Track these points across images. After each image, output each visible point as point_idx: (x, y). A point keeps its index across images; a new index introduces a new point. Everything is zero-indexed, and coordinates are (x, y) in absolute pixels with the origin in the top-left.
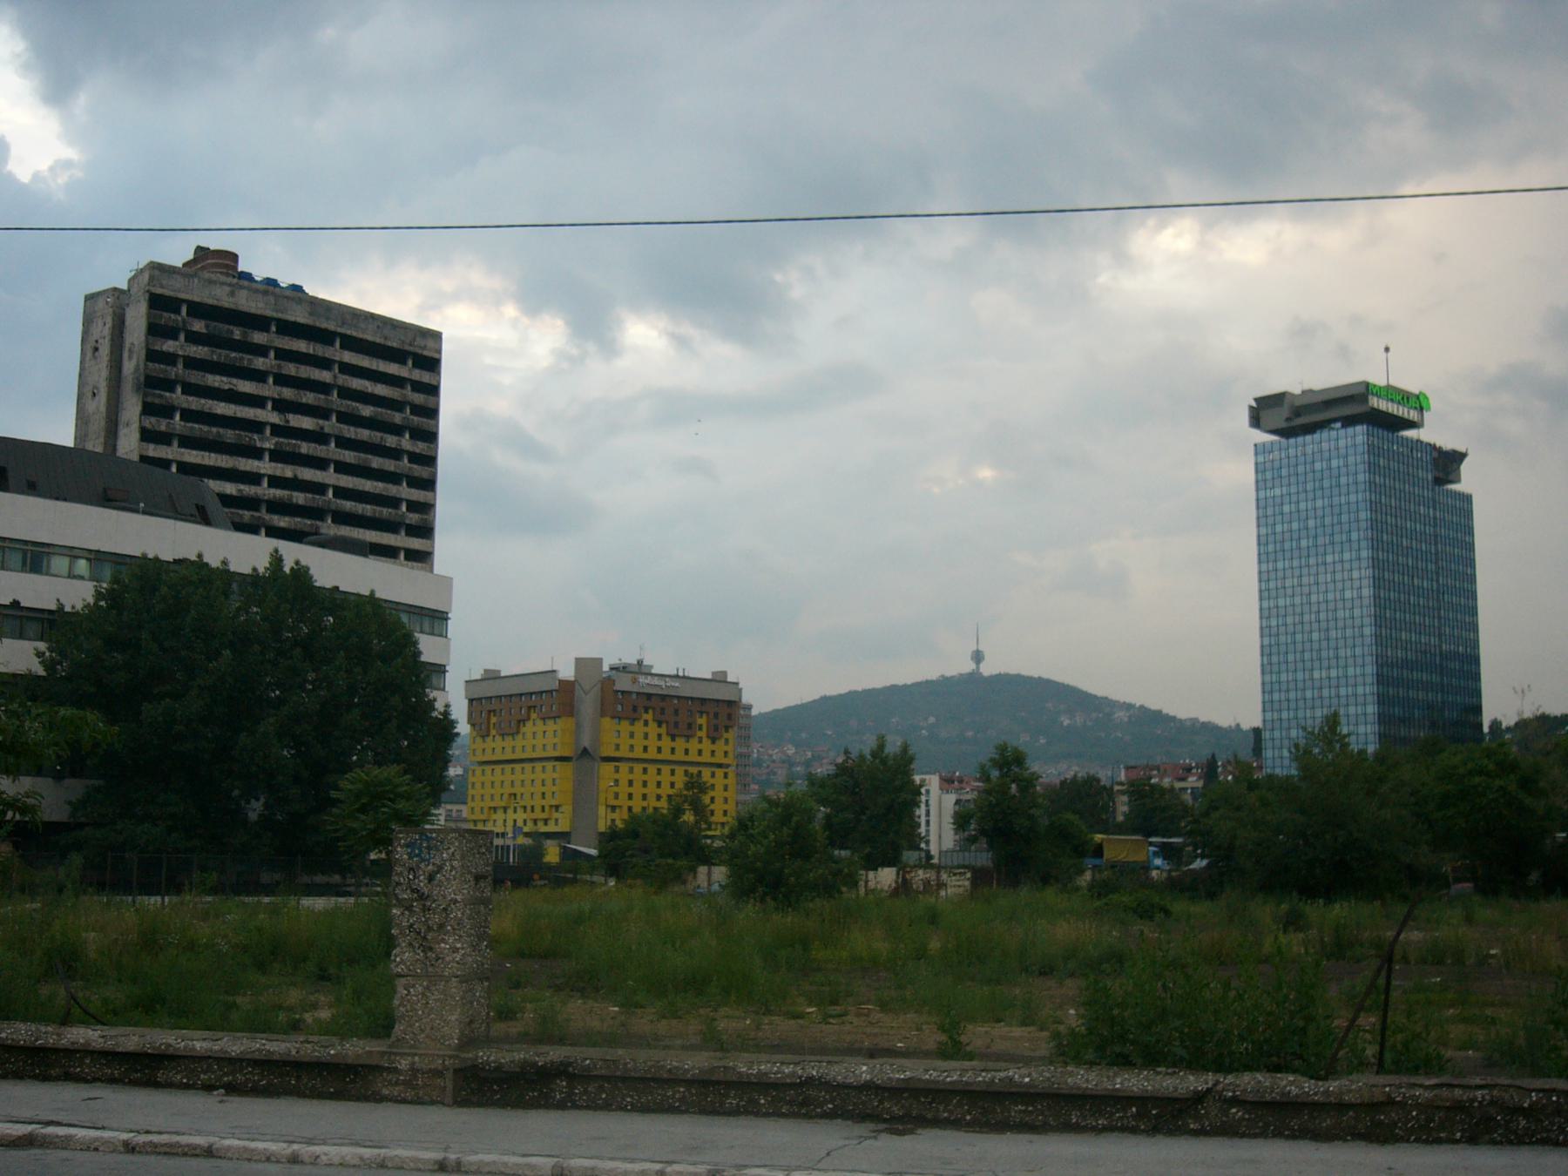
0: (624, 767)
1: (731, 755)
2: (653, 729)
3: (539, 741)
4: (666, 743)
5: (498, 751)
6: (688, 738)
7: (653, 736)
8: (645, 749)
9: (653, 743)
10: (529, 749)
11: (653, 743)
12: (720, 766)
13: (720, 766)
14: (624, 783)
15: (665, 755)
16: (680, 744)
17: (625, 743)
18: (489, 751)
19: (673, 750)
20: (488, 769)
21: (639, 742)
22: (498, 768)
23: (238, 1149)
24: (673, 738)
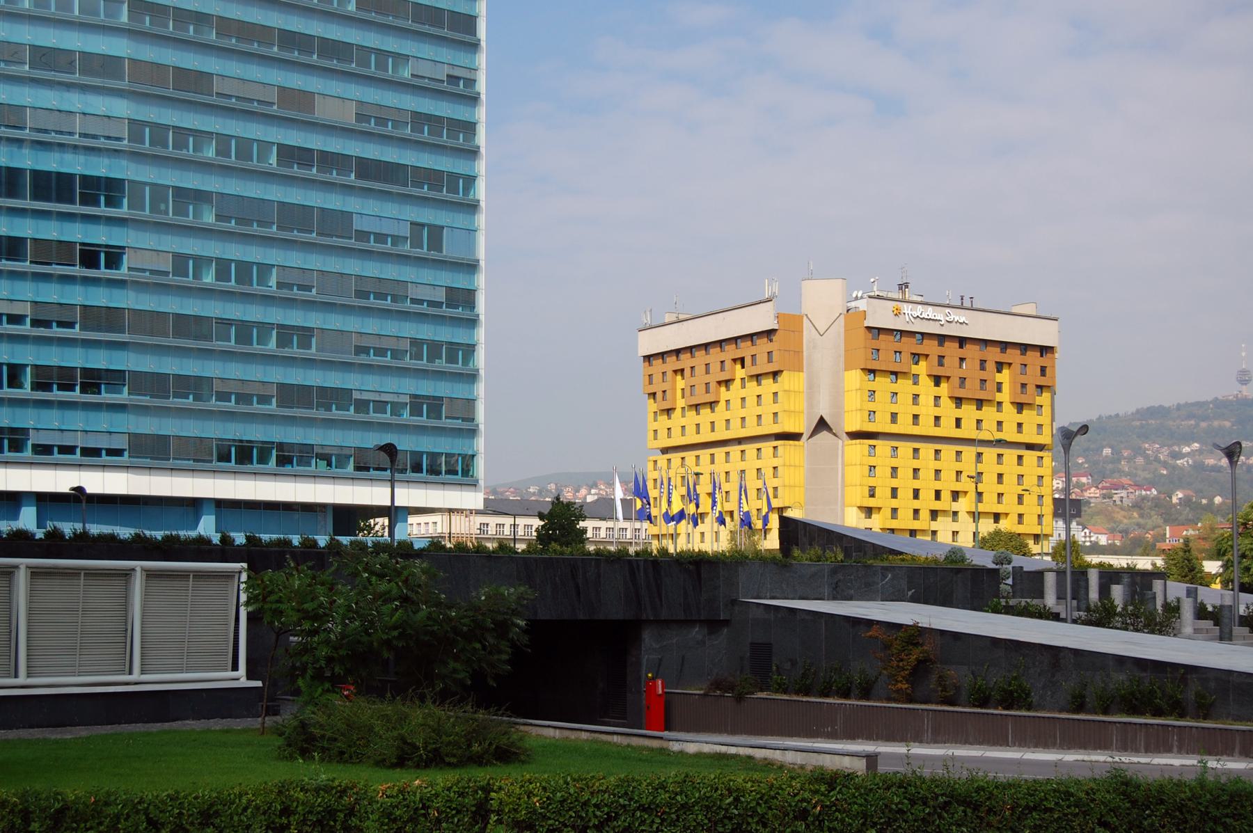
0: (883, 446)
1: (1046, 430)
2: (926, 387)
3: (751, 410)
4: (948, 410)
5: (691, 429)
6: (980, 403)
7: (926, 400)
8: (894, 417)
9: (927, 409)
10: (736, 423)
11: (927, 409)
12: (1030, 447)
13: (1030, 447)
14: (883, 471)
15: (968, 431)
16: (969, 413)
17: (905, 409)
18: (676, 431)
19: (958, 422)
20: (676, 457)
21: (905, 409)
22: (751, 449)
23: (1165, 748)
24: (959, 401)
